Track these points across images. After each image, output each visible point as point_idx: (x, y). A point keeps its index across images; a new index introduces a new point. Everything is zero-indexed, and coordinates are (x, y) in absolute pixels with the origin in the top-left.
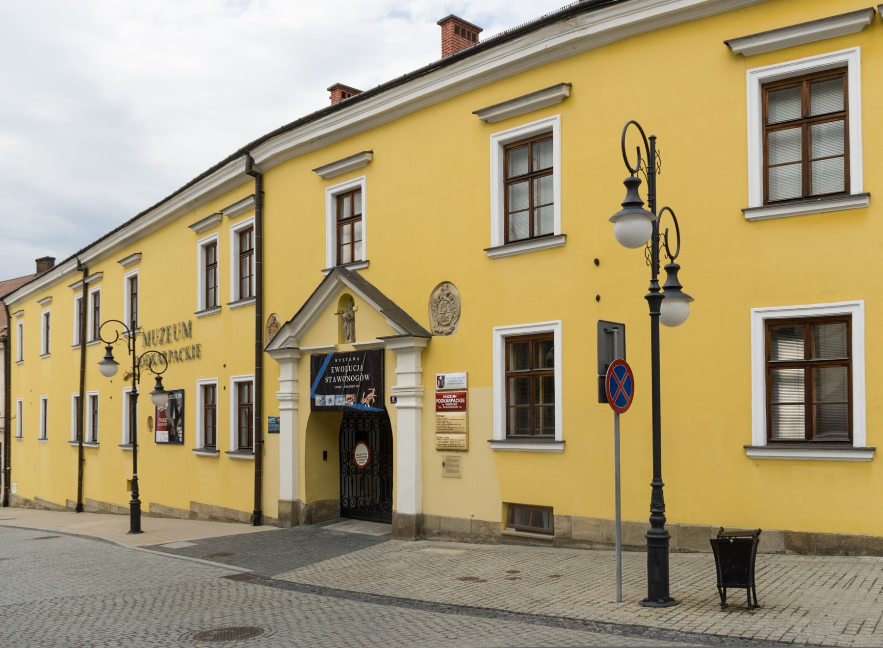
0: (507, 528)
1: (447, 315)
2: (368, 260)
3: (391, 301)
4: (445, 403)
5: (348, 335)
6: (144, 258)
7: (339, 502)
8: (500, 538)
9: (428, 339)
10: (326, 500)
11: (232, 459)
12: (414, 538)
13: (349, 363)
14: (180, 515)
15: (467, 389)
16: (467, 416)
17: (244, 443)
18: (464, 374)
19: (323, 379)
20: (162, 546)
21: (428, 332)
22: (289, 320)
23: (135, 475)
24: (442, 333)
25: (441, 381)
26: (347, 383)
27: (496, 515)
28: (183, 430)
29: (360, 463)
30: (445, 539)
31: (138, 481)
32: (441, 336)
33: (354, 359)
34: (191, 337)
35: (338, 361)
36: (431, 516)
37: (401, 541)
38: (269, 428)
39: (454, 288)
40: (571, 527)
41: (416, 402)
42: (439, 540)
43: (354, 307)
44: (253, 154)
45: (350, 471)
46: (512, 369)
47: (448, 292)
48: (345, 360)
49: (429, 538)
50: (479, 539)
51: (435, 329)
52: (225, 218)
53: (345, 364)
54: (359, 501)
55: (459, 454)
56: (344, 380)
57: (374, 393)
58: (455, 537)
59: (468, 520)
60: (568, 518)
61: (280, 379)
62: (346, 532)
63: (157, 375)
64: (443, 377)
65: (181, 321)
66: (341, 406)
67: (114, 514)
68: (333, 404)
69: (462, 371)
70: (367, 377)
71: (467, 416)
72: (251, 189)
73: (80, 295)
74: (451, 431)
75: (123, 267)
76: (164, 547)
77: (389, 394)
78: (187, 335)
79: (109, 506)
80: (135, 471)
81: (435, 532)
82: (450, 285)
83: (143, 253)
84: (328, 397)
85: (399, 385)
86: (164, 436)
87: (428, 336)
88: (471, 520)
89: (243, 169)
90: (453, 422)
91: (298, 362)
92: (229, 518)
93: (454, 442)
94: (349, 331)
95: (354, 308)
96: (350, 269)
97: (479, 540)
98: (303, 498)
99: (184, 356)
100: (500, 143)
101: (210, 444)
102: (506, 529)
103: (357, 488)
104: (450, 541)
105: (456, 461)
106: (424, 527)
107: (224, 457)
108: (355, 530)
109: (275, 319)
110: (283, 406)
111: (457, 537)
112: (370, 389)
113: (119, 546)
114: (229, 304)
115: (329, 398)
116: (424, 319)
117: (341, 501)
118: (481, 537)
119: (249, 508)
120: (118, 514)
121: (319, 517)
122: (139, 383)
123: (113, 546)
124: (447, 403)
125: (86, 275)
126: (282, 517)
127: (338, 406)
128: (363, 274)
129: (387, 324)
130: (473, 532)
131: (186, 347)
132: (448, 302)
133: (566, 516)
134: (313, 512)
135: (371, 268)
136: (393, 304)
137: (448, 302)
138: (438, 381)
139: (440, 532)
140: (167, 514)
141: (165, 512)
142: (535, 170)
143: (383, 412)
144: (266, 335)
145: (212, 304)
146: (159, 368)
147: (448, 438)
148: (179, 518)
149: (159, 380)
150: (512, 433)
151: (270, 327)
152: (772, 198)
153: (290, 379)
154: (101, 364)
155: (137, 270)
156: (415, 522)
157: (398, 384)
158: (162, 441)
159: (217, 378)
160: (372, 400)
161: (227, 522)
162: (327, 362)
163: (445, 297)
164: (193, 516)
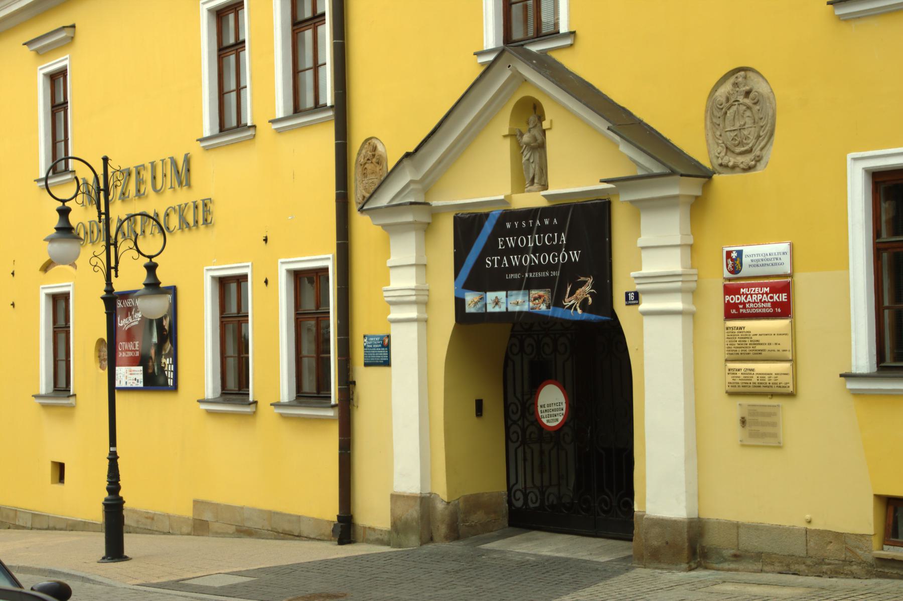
0: (886, 547)
1: (746, 132)
2: (572, 30)
3: (624, 109)
4: (744, 304)
5: (531, 176)
7: (505, 497)
8: (872, 565)
9: (707, 179)
10: (483, 494)
11: (283, 416)
12: (684, 566)
13: (535, 229)
14: (171, 527)
15: (790, 275)
16: (793, 327)
17: (309, 386)
18: (784, 247)
19: (480, 261)
20: (186, 582)
21: (705, 167)
22: (411, 150)
23: (112, 449)
24: (734, 168)
25: (735, 262)
26: (532, 269)
28: (175, 363)
29: (548, 421)
30: (750, 567)
32: (732, 173)
33: (547, 222)
34: (189, 185)
35: (513, 225)
36: (719, 523)
37: (660, 571)
38: (366, 355)
39: (761, 79)
41: (683, 302)
42: (736, 570)
43: (544, 123)
45: (527, 437)
46: (885, 237)
47: (747, 88)
48: (527, 223)
49: (715, 566)
50: (825, 568)
51: (720, 161)
53: (528, 231)
54: (547, 494)
55: (775, 401)
56: (526, 263)
57: (590, 286)
58: (772, 564)
59: (799, 530)
61: (390, 263)
62: (535, 555)
64: (740, 253)
65: (166, 156)
66: (520, 313)
67: (24, 528)
68: (503, 309)
69: (779, 241)
70: (575, 256)
71: (793, 327)
74: (758, 356)
75: (33, 53)
76: (185, 584)
77: (620, 288)
78: (180, 184)
79: (12, 514)
80: (113, 442)
81: (727, 553)
82: (750, 74)
83: (76, 25)
84: (491, 296)
85: (646, 270)
86: (134, 377)
87: (705, 175)
88: (806, 530)
90: (762, 339)
91: (426, 229)
92: (280, 531)
93: (767, 378)
94: (534, 168)
95: (545, 125)
96: (535, 48)
97: (824, 570)
98: (441, 489)
99: (174, 221)
102: (883, 549)
103: (533, 471)
104: (762, 571)
105: (770, 415)
106: (704, 545)
108: (551, 551)
109: (375, 149)
110: (396, 313)
111: (777, 564)
112: (582, 279)
113: (100, 583)
114: (273, 121)
115: (494, 298)
117: (509, 495)
118: (829, 564)
120: (31, 529)
121: (471, 526)
122: (116, 276)
123: (88, 585)
126: (399, 528)
127: (513, 313)
128: (567, 60)
129: (621, 152)
130: (811, 553)
131: (180, 206)
132: (749, 108)
134: (461, 516)
135: (577, 47)
136: (629, 114)
137: (749, 108)
138: (729, 260)
139: (738, 553)
140: (141, 526)
141: (138, 521)
143: (608, 322)
144: (356, 180)
146: (151, 244)
147: (753, 370)
148: (169, 533)
149: (151, 268)
150: (889, 362)
151: (365, 164)
153: (413, 262)
154: (51, 240)
155: (66, 59)
156: (685, 536)
157: (643, 267)
158: (129, 385)
159: (249, 264)
160: (586, 300)
161: (276, 539)
162: (488, 228)
163: (741, 99)
164: (200, 527)
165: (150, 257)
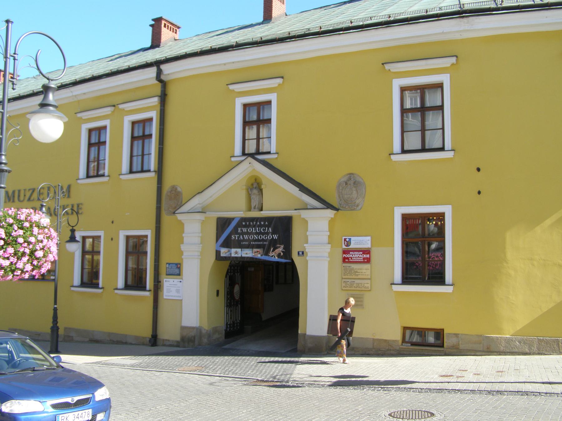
4: (351, 258)
26: (256, 240)
27: (396, 335)
31: (58, 311)
40: (459, 342)
57: (282, 248)
60: (456, 335)
63: (71, 228)
64: (350, 239)
80: (55, 303)
84: (233, 250)
124: (354, 257)
133: (454, 334)
152: (405, 149)
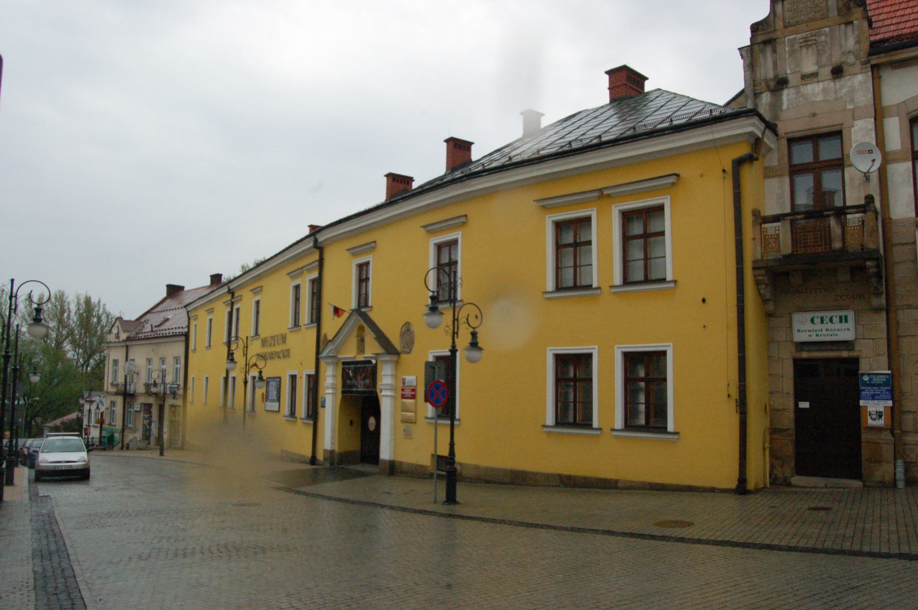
6: (264, 289)
16: (416, 402)
25: (404, 381)
36: (398, 462)
44: (318, 236)
52: (305, 272)
71: (416, 402)
72: (316, 257)
73: (229, 309)
89: (311, 244)
99: (281, 355)
100: (553, 222)
101: (292, 414)
107: (299, 421)
116: (396, 342)
119: (308, 453)
122: (457, 337)
125: (233, 297)
142: (578, 241)
145: (297, 324)
154: (427, 315)
165: (474, 328)
